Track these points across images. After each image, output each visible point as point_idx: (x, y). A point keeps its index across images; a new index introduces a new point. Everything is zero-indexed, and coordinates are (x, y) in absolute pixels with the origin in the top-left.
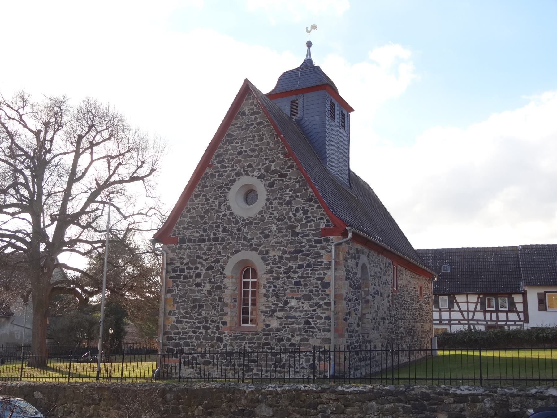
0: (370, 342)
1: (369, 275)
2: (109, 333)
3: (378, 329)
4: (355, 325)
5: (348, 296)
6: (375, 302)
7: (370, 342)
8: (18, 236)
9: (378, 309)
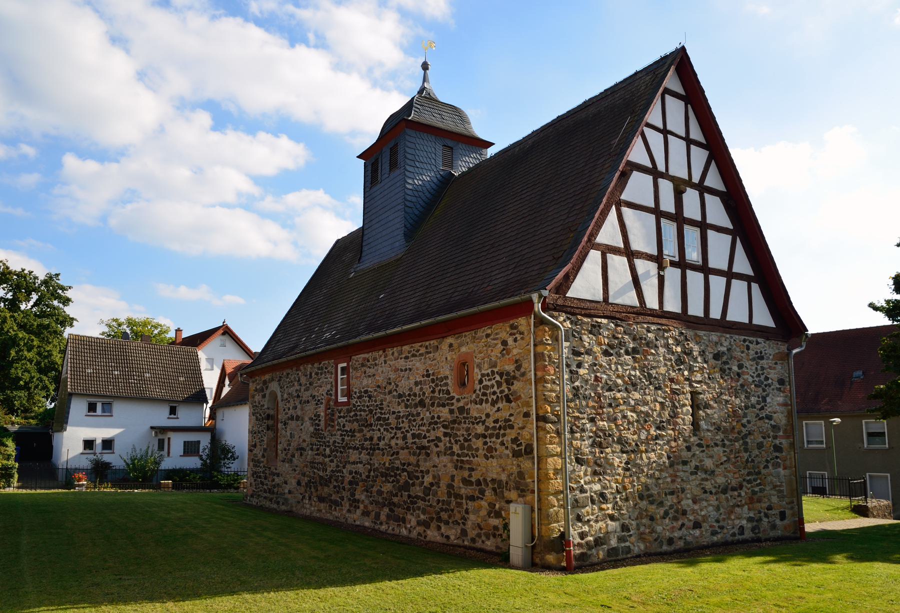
0: (278, 475)
1: (746, 338)
2: (549, 553)
3: (291, 461)
4: (260, 455)
5: (254, 429)
6: (288, 429)
7: (278, 475)
8: (826, 415)
9: (291, 437)
